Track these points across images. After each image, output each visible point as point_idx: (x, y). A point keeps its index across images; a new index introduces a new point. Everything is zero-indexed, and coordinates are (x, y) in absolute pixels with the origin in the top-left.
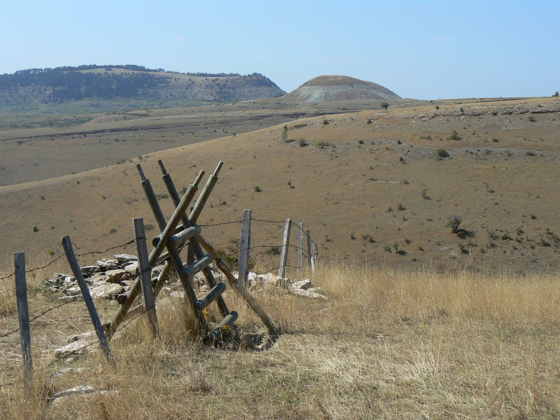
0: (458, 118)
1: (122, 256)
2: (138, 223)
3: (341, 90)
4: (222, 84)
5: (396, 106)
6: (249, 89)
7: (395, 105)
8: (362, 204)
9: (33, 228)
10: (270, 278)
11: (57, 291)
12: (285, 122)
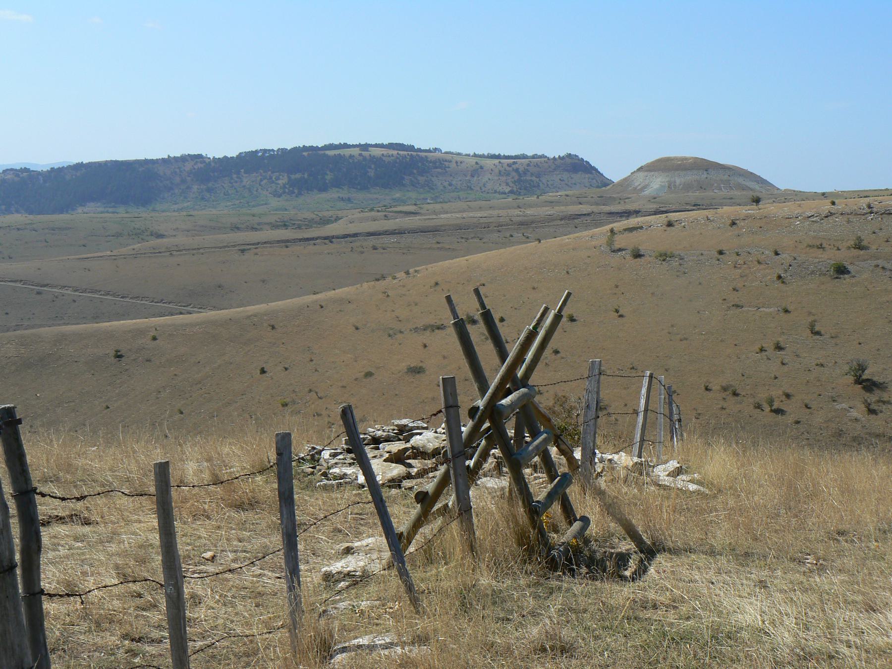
0: (863, 217)
1: (404, 422)
2: (449, 384)
3: (690, 177)
4: (521, 169)
5: (771, 201)
6: (559, 177)
7: (769, 199)
8: (722, 341)
9: (259, 368)
10: (624, 459)
11: (312, 473)
12: (611, 223)
